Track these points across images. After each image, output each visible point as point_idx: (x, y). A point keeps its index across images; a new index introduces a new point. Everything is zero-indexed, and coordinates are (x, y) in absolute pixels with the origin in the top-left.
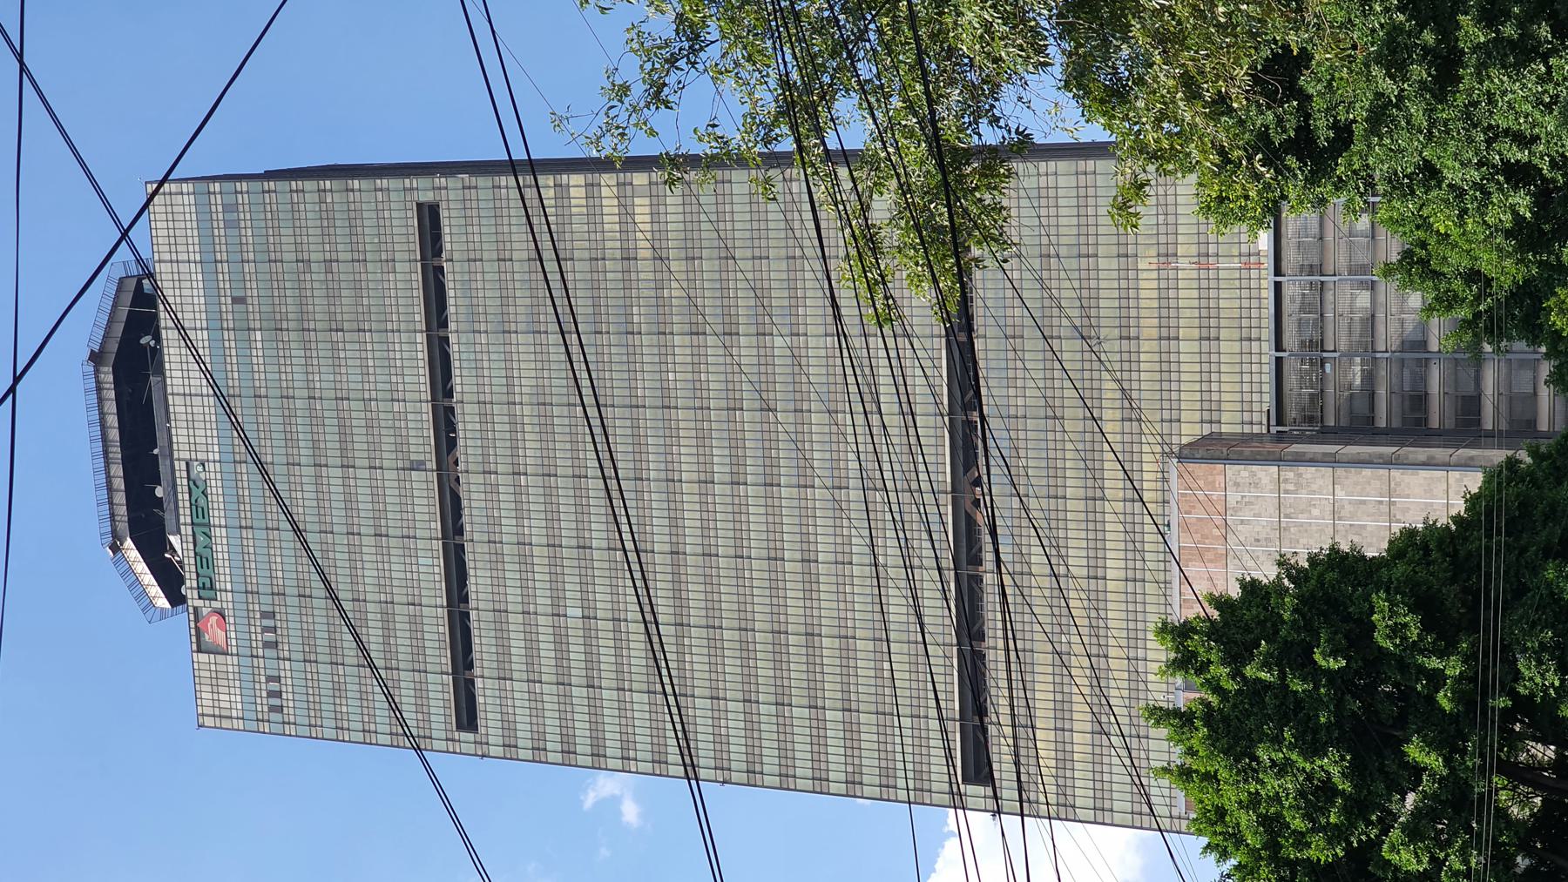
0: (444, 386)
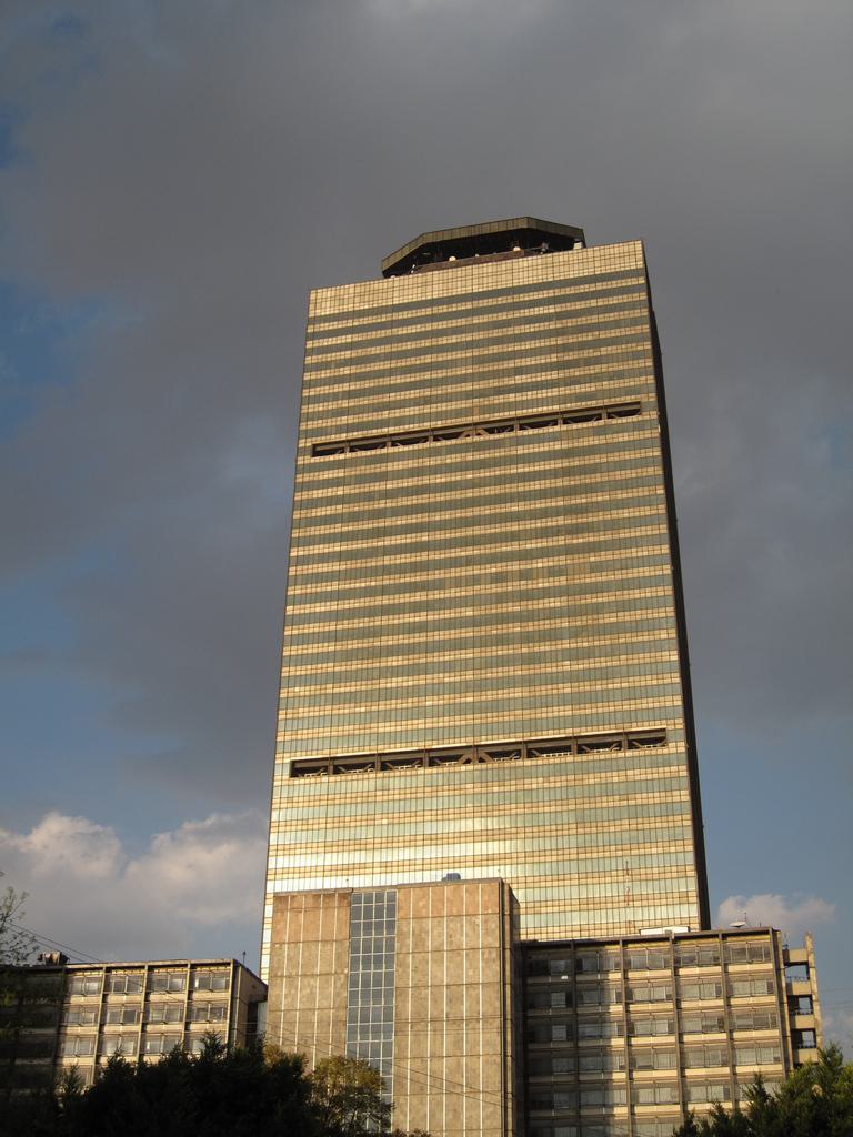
0: (356, 447)
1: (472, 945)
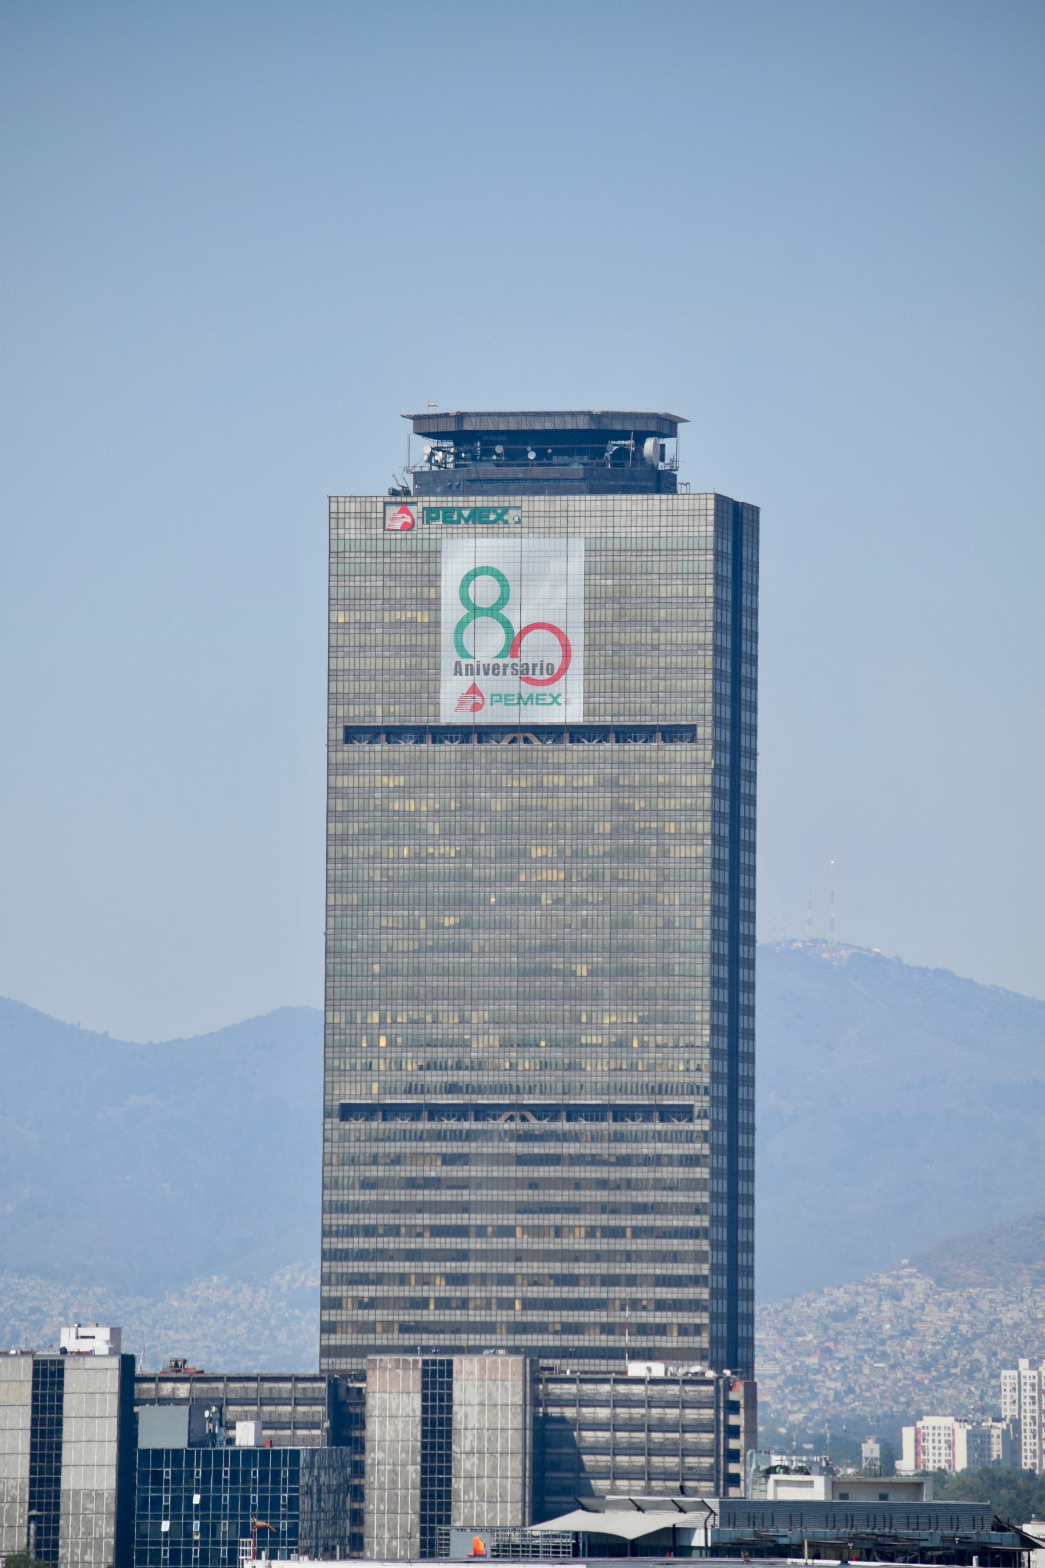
1: (504, 1402)
